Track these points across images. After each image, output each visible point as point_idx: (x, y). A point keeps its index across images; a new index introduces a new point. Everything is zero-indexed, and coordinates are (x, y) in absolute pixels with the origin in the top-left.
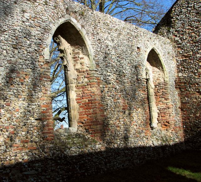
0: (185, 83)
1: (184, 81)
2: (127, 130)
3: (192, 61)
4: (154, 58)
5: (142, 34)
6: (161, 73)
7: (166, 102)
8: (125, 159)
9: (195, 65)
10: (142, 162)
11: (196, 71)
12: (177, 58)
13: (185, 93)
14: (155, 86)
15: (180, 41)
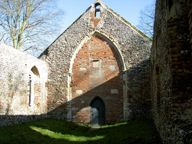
0: (51, 84)
1: (50, 83)
2: (9, 106)
3: (55, 74)
4: (35, 70)
5: (29, 58)
6: (38, 78)
7: (39, 93)
8: (9, 121)
9: (56, 76)
10: (20, 123)
11: (56, 79)
12: (48, 72)
13: (50, 90)
14: (35, 84)
15: (51, 63)
